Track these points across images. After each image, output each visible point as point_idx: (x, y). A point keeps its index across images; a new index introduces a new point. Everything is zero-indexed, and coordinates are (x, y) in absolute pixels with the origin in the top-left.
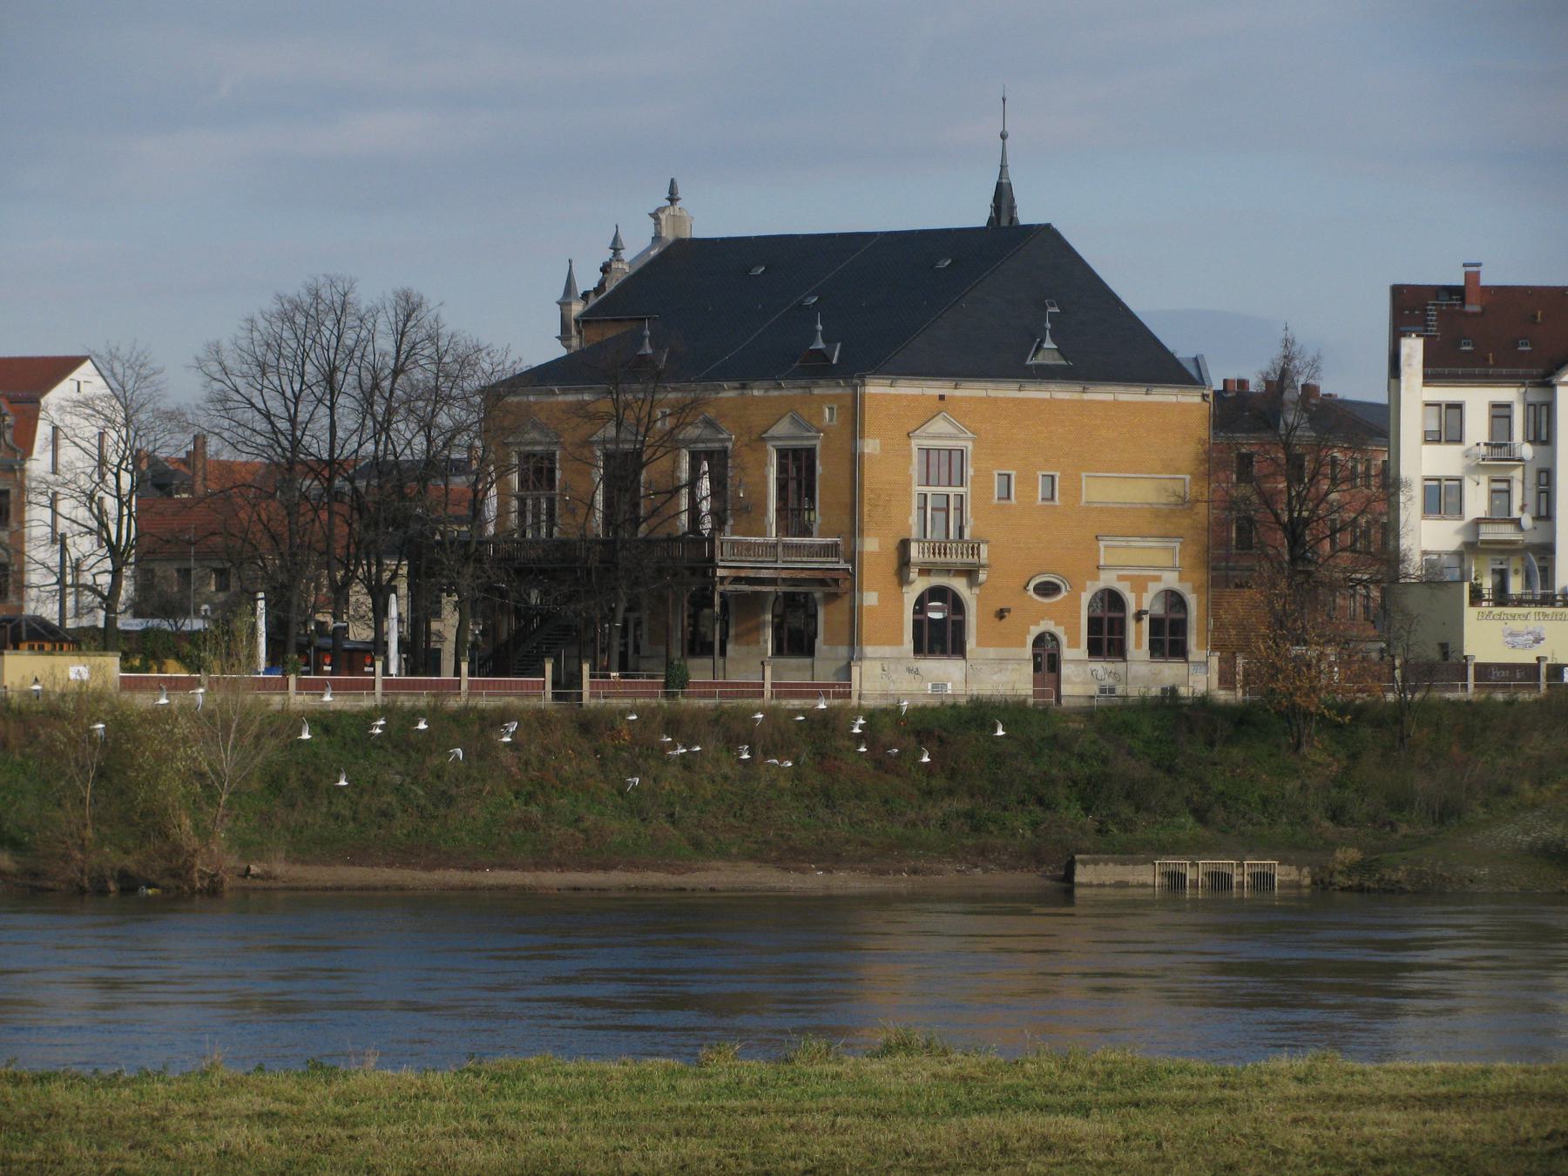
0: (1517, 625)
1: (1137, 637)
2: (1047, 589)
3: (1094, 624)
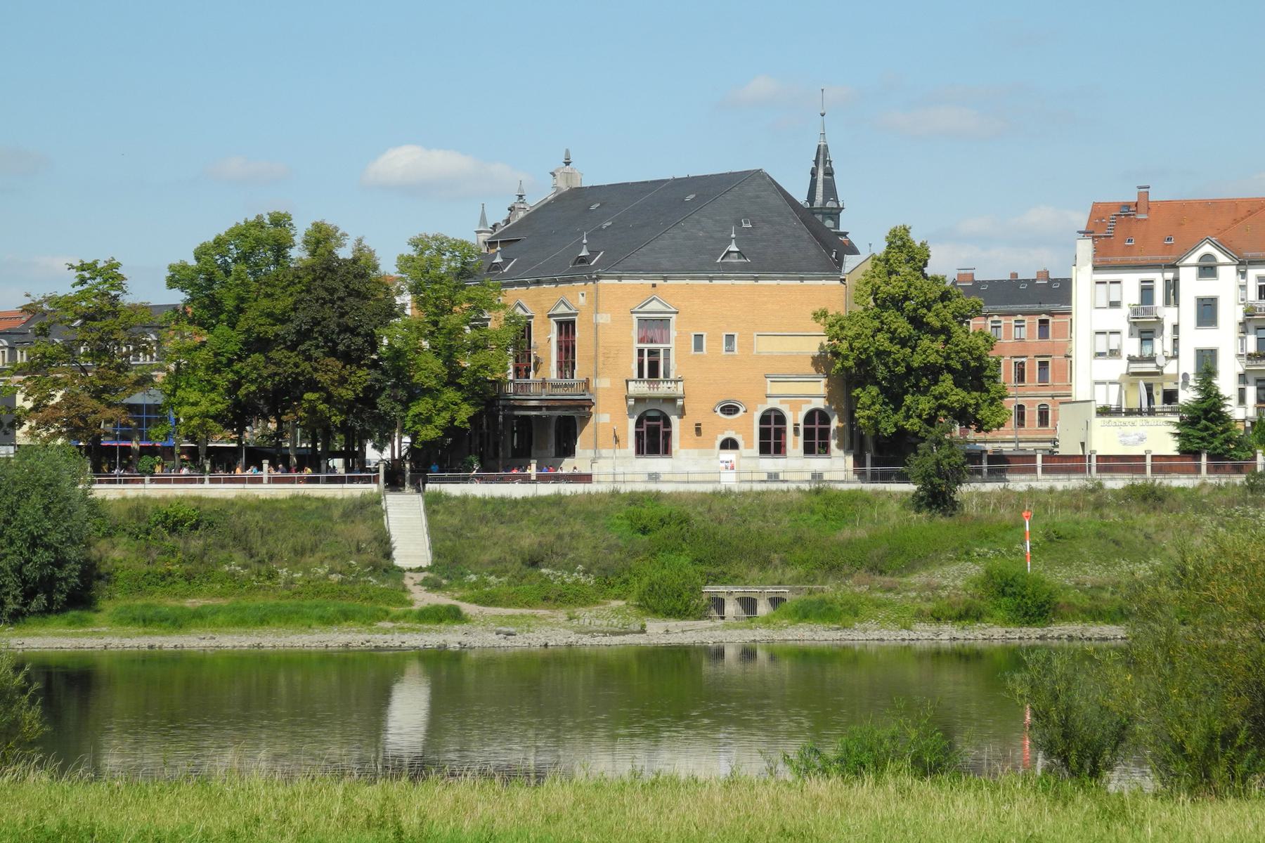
0: (1128, 429)
1: (795, 443)
2: (730, 409)
3: (764, 434)
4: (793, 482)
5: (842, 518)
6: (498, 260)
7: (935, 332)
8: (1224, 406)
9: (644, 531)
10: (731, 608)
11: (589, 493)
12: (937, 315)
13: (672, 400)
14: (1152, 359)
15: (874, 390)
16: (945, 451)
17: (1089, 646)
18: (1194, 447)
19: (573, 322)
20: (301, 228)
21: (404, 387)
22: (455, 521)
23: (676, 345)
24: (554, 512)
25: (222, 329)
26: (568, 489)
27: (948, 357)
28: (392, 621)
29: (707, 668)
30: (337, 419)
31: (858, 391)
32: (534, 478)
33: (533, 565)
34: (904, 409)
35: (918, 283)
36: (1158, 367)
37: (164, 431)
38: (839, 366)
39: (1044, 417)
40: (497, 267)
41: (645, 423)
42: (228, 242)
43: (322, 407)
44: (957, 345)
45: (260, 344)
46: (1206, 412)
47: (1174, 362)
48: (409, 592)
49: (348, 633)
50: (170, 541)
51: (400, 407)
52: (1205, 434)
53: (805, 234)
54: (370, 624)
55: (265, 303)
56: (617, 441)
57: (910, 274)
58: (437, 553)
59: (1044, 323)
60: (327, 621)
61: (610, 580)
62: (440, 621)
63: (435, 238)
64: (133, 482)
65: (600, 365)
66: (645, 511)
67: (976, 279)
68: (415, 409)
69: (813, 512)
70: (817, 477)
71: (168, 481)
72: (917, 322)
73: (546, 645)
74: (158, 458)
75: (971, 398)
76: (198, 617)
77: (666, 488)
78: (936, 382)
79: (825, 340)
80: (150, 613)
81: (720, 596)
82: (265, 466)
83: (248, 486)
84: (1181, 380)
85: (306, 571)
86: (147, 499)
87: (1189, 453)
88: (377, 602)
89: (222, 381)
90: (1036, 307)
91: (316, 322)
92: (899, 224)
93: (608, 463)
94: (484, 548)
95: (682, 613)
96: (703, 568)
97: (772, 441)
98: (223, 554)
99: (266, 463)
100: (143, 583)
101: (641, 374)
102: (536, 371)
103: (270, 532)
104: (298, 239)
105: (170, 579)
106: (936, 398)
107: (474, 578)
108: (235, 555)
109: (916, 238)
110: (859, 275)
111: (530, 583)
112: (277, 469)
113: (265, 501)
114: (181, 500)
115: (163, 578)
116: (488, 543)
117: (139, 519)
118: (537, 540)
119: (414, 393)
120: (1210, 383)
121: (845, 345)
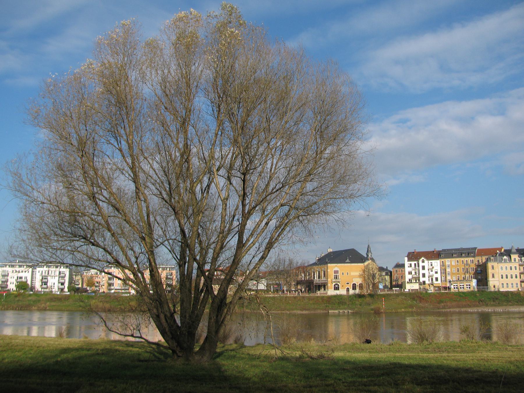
2: (348, 283)
3: (353, 287)
17: (341, 307)
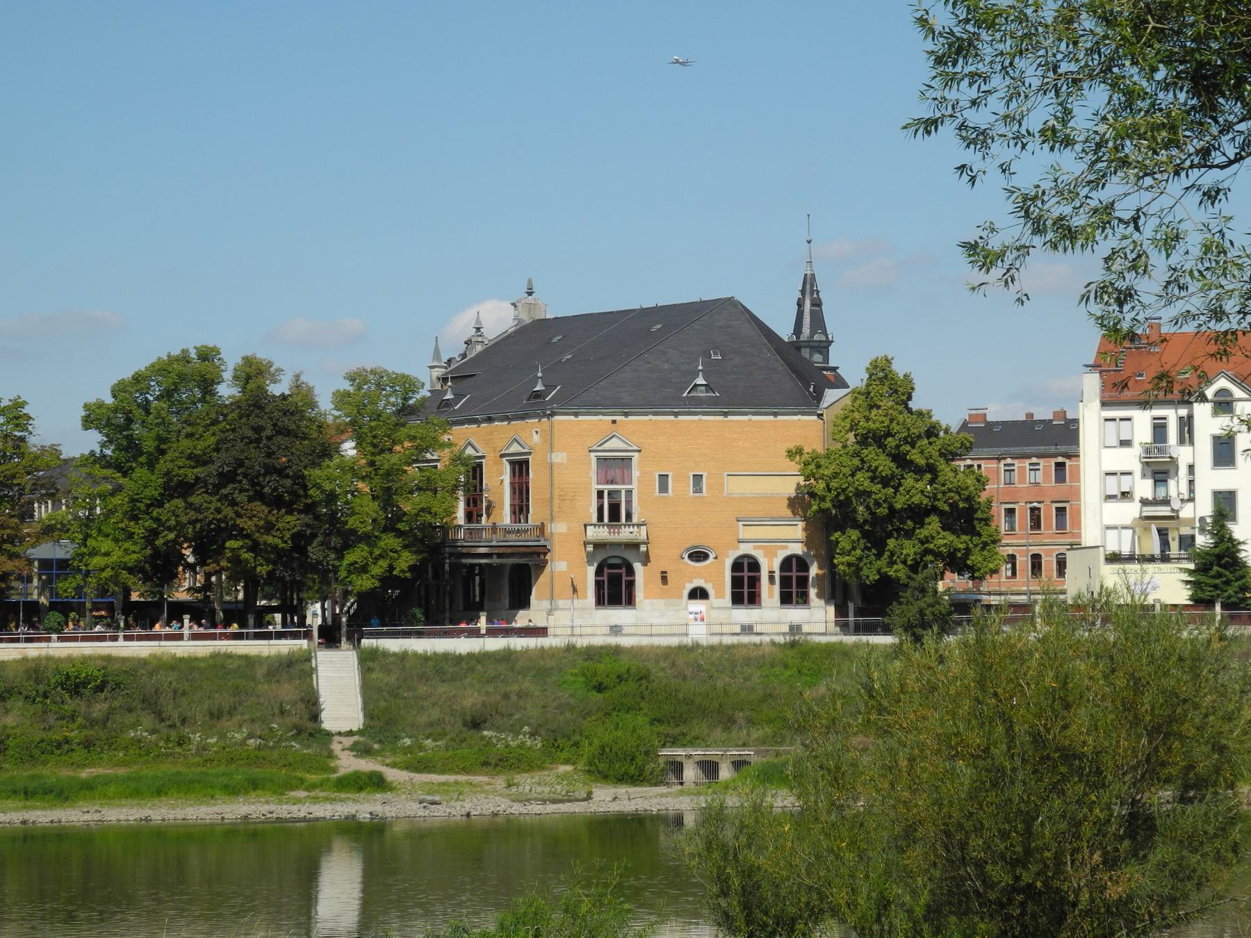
1: (770, 592)
2: (699, 556)
3: (736, 582)
4: (768, 634)
5: (818, 673)
6: (449, 396)
7: (919, 471)
8: (1239, 551)
9: (600, 688)
10: (690, 773)
11: (542, 648)
12: (922, 452)
13: (635, 546)
14: (1166, 502)
15: (854, 534)
16: (929, 599)
18: (1206, 595)
19: (527, 462)
20: (231, 360)
21: (340, 533)
22: (392, 679)
23: (638, 486)
24: (502, 668)
25: (141, 473)
26: (518, 643)
27: (935, 498)
28: (307, 789)
29: (664, 839)
30: (263, 570)
31: (837, 534)
32: (483, 631)
33: (476, 726)
34: (887, 554)
35: (901, 418)
36: (1173, 510)
37: (74, 585)
38: (815, 508)
39: (1062, 565)
40: (448, 404)
41: (606, 571)
42: (149, 378)
43: (247, 556)
44: (944, 485)
45: (183, 489)
46: (1219, 557)
47: (1190, 505)
48: (337, 757)
49: (253, 804)
50: (71, 705)
51: (333, 556)
52: (1218, 581)
53: (790, 368)
54: (282, 794)
55: (185, 443)
56: (575, 590)
57: (892, 408)
58: (369, 714)
59: (1061, 466)
60: (232, 791)
61: (558, 743)
62: (361, 789)
63: (373, 372)
64: (39, 640)
65: (556, 509)
66: (601, 667)
67: (989, 419)
68: (350, 557)
69: (786, 667)
70: (795, 629)
71: (75, 639)
72: (900, 459)
73: (468, 815)
74: (72, 615)
75: (961, 542)
76: (88, 788)
77: (625, 642)
78: (922, 525)
79: (801, 480)
80: (32, 786)
81: (679, 759)
82: (186, 622)
83: (163, 643)
84: (1198, 525)
85: (222, 736)
86: (49, 658)
87: (1202, 601)
88: (295, 769)
89: (138, 530)
90: (1052, 449)
91: (241, 464)
92: (881, 355)
93: (566, 616)
94: (422, 709)
95: (636, 778)
96: (661, 728)
97: (746, 590)
98: (130, 719)
99: (186, 619)
100: (36, 752)
101: (600, 518)
102: (489, 516)
103: (184, 694)
104: (228, 375)
105: (66, 747)
106: (922, 543)
107: (408, 741)
108: (142, 719)
109: (899, 369)
110: (837, 410)
111: (470, 746)
112: (200, 625)
113: (181, 660)
114: (86, 660)
115: (59, 746)
116: (425, 703)
117: (38, 681)
118: (481, 699)
119: (350, 539)
120: (1223, 526)
121: (822, 484)
